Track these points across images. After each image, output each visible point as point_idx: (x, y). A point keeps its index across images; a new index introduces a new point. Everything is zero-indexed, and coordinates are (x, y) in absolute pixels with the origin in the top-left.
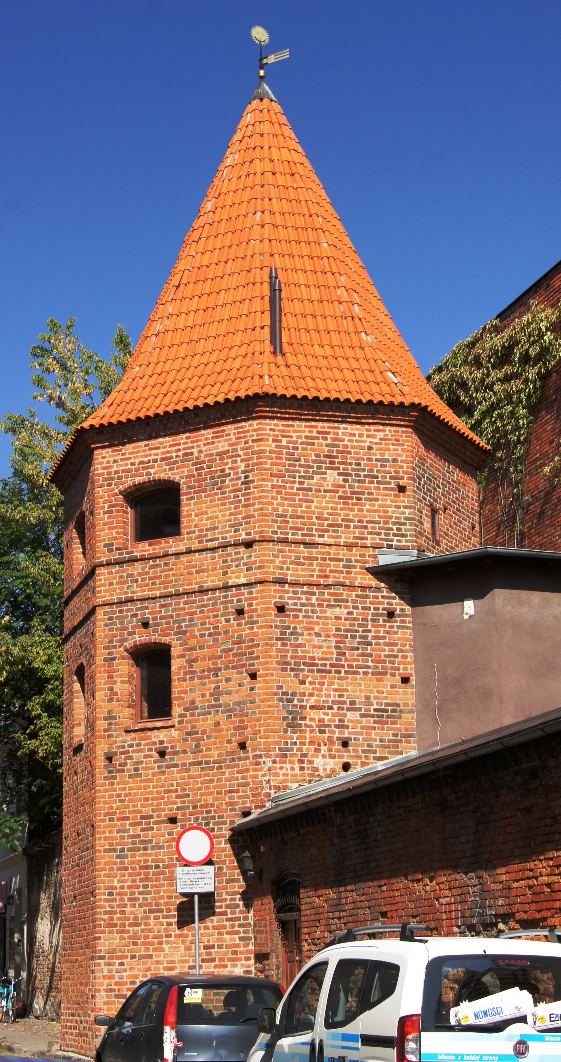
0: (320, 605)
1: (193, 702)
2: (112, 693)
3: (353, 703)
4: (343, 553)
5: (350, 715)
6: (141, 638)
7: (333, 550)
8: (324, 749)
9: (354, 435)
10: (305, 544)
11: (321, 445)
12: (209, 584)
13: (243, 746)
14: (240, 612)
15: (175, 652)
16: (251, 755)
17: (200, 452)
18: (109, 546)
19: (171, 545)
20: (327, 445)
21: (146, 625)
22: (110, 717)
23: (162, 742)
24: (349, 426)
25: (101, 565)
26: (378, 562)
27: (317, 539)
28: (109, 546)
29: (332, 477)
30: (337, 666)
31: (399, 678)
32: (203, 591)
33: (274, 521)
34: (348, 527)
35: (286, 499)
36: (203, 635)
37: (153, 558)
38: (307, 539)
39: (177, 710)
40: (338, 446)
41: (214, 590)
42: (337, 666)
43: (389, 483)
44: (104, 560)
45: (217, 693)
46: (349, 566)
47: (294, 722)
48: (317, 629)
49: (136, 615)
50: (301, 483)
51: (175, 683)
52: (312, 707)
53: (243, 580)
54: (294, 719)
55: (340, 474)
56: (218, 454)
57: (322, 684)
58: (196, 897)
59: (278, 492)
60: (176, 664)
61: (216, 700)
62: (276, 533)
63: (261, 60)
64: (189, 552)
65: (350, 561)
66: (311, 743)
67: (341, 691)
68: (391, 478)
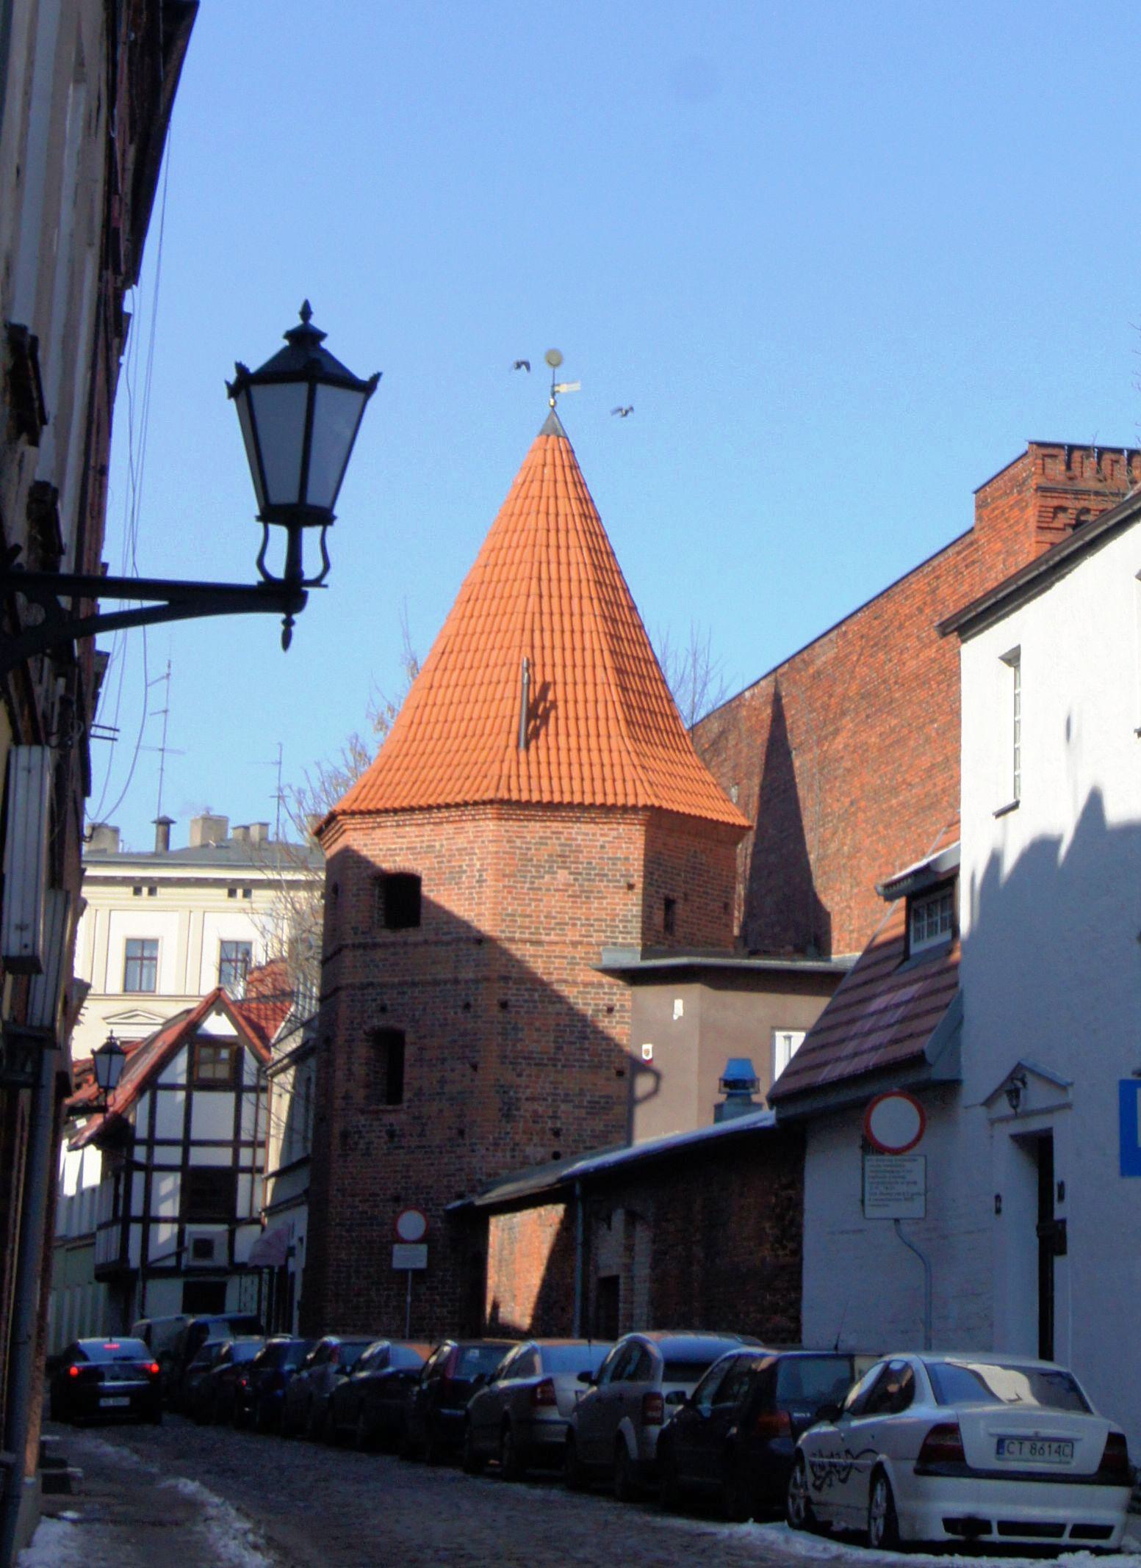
0: (543, 1002)
1: (421, 1089)
2: (350, 1073)
3: (567, 1095)
4: (568, 951)
5: (563, 1107)
6: (377, 1022)
7: (557, 948)
8: (536, 1139)
9: (587, 834)
10: (532, 943)
11: (554, 845)
12: (441, 976)
13: (461, 1133)
14: (467, 1006)
15: (409, 1038)
16: (467, 1142)
17: (442, 846)
18: (355, 929)
19: (412, 935)
20: (561, 845)
21: (383, 1009)
22: (347, 1097)
23: (391, 1125)
24: (583, 826)
25: (346, 946)
26: (1132, 453)
27: (544, 938)
28: (355, 929)
29: (562, 876)
30: (554, 1060)
31: (614, 1071)
32: (436, 983)
33: (504, 920)
34: (574, 925)
35: (515, 899)
36: (433, 1025)
37: (393, 944)
38: (534, 938)
39: (407, 1095)
40: (570, 845)
41: (445, 982)
42: (554, 1060)
43: (618, 881)
44: (349, 942)
45: (442, 1082)
46: (573, 963)
47: (508, 1111)
48: (537, 1024)
49: (375, 1000)
50: (532, 883)
51: (407, 1069)
52: (527, 1099)
53: (471, 976)
54: (509, 1109)
55: (571, 873)
56: (458, 850)
57: (538, 1077)
58: (410, 1274)
59: (510, 892)
60: (409, 1051)
61: (442, 1088)
62: (503, 932)
63: (554, 386)
64: (426, 942)
65: (574, 958)
66: (524, 1132)
67: (555, 1084)
68: (622, 876)
